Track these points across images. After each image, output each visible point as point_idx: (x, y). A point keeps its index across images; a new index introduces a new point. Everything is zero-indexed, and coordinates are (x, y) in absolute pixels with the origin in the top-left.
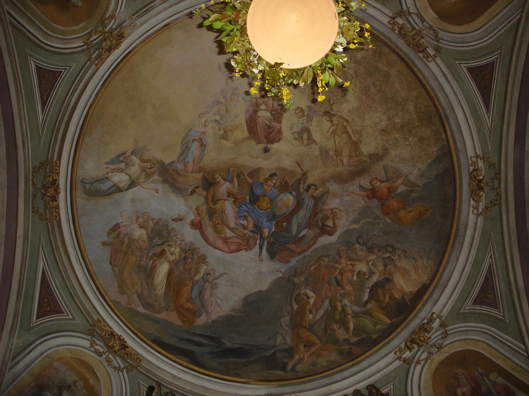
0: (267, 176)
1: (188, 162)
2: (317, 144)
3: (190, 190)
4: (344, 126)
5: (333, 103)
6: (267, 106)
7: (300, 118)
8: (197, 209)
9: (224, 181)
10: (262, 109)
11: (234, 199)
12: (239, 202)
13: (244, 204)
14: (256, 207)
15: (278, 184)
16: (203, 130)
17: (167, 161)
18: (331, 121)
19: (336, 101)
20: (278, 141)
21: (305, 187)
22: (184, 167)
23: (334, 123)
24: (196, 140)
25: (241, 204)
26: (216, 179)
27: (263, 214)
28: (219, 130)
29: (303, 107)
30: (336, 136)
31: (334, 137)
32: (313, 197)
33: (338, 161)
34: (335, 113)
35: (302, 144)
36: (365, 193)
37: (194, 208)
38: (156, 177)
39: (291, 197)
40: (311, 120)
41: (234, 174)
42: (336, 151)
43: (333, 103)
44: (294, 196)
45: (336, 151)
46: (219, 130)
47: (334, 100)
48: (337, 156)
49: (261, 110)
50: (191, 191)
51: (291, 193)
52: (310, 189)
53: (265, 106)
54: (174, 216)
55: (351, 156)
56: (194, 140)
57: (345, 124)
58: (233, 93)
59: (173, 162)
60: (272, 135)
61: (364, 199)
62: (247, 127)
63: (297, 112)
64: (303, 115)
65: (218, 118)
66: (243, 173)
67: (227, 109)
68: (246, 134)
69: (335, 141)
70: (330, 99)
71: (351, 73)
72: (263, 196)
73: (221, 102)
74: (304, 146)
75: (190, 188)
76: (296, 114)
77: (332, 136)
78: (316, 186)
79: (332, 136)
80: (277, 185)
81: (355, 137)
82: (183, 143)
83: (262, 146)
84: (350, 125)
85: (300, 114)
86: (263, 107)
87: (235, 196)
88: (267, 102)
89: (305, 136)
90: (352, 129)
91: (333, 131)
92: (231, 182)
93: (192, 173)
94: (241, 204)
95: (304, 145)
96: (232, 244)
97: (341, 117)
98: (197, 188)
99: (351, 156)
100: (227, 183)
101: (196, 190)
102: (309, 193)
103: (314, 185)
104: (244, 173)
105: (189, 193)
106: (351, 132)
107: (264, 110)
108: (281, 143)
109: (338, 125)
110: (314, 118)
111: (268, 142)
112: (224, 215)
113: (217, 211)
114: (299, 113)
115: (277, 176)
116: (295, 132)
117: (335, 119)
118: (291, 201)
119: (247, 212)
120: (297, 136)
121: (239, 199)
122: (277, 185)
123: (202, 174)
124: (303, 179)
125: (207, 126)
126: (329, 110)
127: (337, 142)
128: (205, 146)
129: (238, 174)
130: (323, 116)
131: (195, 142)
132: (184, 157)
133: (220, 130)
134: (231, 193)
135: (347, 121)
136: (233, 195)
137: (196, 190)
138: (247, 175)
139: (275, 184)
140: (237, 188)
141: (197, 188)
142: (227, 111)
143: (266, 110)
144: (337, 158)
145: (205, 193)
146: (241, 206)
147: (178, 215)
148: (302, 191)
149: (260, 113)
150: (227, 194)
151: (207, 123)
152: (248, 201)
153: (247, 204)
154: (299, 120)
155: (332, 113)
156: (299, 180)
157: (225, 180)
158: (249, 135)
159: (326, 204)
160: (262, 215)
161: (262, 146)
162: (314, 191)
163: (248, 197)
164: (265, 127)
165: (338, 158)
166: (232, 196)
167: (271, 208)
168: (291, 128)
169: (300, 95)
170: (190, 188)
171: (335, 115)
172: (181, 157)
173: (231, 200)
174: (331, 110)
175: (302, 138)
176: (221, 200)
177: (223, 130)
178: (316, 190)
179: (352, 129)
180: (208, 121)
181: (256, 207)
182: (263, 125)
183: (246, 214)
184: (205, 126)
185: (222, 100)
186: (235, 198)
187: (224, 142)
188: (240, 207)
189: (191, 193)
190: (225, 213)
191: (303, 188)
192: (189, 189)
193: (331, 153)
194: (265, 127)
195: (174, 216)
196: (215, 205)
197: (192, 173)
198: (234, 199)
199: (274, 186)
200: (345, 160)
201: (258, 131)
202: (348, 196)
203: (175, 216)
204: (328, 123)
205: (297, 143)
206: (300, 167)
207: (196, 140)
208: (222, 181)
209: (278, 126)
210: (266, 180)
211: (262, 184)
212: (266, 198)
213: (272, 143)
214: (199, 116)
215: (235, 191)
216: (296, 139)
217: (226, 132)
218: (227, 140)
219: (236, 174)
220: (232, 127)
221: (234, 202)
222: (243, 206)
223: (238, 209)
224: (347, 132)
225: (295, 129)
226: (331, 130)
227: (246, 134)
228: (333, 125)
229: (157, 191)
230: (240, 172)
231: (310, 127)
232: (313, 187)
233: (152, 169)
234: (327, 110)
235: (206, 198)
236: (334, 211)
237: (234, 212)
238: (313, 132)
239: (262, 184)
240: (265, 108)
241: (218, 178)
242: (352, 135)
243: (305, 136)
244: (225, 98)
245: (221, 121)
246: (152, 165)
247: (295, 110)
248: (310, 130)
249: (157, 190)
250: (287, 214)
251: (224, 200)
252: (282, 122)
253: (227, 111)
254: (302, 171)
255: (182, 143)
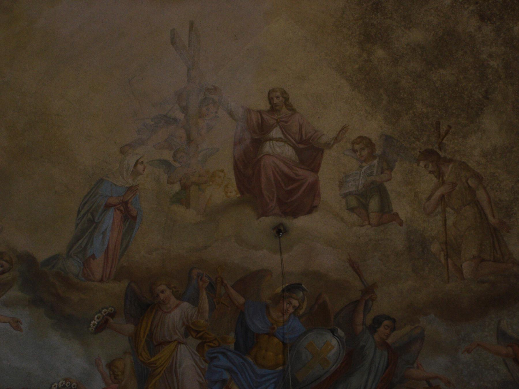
0: (279, 290)
1: (93, 257)
2: (401, 224)
3: (95, 322)
4: (469, 187)
5: (447, 132)
6: (285, 130)
7: (365, 161)
8: (110, 365)
9: (178, 298)
10: (275, 136)
11: (199, 341)
12: (211, 347)
13: (224, 354)
14: (250, 359)
15: (304, 308)
16: (131, 182)
17: (42, 256)
18: (440, 175)
19: (453, 129)
20: (310, 212)
21: (369, 322)
22: (82, 267)
23: (445, 179)
24: (115, 206)
25: (214, 353)
26: (158, 295)
27: (266, 378)
28: (169, 182)
29: (374, 137)
30: (448, 209)
31: (444, 211)
32: (385, 345)
33: (450, 267)
34: (449, 157)
35: (367, 222)
36: (510, 349)
37: (103, 363)
38: (15, 293)
39: (334, 342)
40: (391, 169)
41: (201, 283)
42: (446, 243)
43: (447, 132)
44: (339, 338)
45: (446, 243)
46: (169, 182)
47: (450, 127)
48: (447, 256)
49: (271, 139)
50: (98, 323)
51: (333, 332)
52: (379, 327)
53: (280, 132)
54: (56, 384)
55: (483, 260)
56: (108, 206)
57: (472, 182)
58: (205, 98)
59: (56, 258)
60: (293, 199)
61: (506, 364)
62: (236, 175)
63: (357, 147)
64: (372, 156)
65: (167, 155)
66: (222, 282)
67: (189, 137)
68: (234, 193)
69: (445, 221)
70: (438, 123)
71: (496, 66)
72: (267, 334)
73: (175, 120)
74: (369, 226)
75: (96, 316)
76: (355, 151)
77: (439, 209)
78: (394, 321)
79: (439, 209)
80: (301, 312)
81: (494, 216)
82: (82, 214)
83: (269, 221)
84: (485, 188)
85: (365, 153)
86: (276, 133)
87: (201, 334)
88: (286, 122)
89: (374, 204)
90: (489, 197)
91: (442, 197)
92: (195, 301)
93: (101, 281)
94: (214, 353)
95: (370, 224)
96: (136, 192)
97: (464, 166)
98: (112, 315)
99: (483, 260)
100: (186, 305)
101: (111, 320)
102: (376, 336)
103: (389, 318)
104: (225, 282)
105: (92, 327)
106: (485, 204)
107: (278, 140)
108: (316, 216)
109: (454, 185)
110: (397, 164)
111: (285, 214)
112: (175, 380)
113: (159, 370)
114: (362, 149)
115: (303, 290)
116: (350, 194)
117: (448, 170)
118: (333, 351)
119: (229, 370)
120: (354, 203)
121: (210, 342)
122: (301, 312)
123: (125, 284)
124: (364, 302)
125: (141, 174)
126: (436, 147)
127: (450, 222)
128: (135, 218)
129: (210, 283)
130: (418, 161)
131: (112, 209)
132: (83, 246)
133: (173, 183)
134: (192, 326)
135: (478, 177)
136: (198, 332)
137: (111, 320)
138: (233, 287)
139: (297, 309)
140: (207, 315)
141: (112, 315)
142: (190, 140)
143: (282, 141)
144: (447, 260)
145: (130, 328)
146: (215, 357)
147: (66, 380)
148: (360, 328)
149: (267, 147)
150: (183, 329)
151: (140, 167)
152: (232, 347)
153: (229, 353)
154: (361, 167)
155: (442, 154)
156: (356, 303)
157: (180, 297)
158: (239, 195)
159: (415, 365)
160: (264, 379)
161: (269, 221)
162: (388, 331)
163: (232, 337)
164: (280, 179)
165: (449, 260)
166: (194, 335)
167: (284, 364)
168: (341, 184)
169: (366, 110)
170: (96, 316)
171: (450, 161)
172: (78, 244)
173: (193, 342)
174: (440, 149)
175: (365, 207)
176: (170, 342)
177: (179, 183)
178: (393, 329)
179: (489, 197)
180: (142, 162)
181: (250, 359)
182: (273, 173)
183: (226, 376)
184: (135, 173)
185: (181, 116)
186: (201, 338)
187: (179, 210)
188: (212, 359)
189: (96, 328)
190: (176, 373)
191: (364, 323)
192: (93, 319)
193: (435, 248)
194: (280, 179)
195: (56, 384)
196: (154, 356)
197: (101, 281)
198: (199, 341)
199: (294, 313)
200: (467, 267)
201: (263, 186)
202: (469, 351)
203: (58, 383)
204: (432, 176)
205: (353, 218)
206: (357, 273)
207: (115, 206)
208: (173, 301)
209: (310, 178)
210: (278, 299)
211: (267, 307)
212: (276, 340)
213: (295, 214)
214: (123, 151)
215: (202, 321)
216: (352, 210)
217: (185, 187)
218: (188, 205)
219: (206, 285)
220: (200, 176)
221: (200, 348)
222: (221, 356)
223: (207, 365)
224: (476, 203)
225: (351, 187)
226: (438, 194)
227: (234, 193)
228: (443, 183)
229: (16, 324)
230: (216, 279)
231: (386, 184)
232: (386, 322)
233: (7, 275)
234: (430, 147)
235: (134, 338)
236: (432, 382)
237: (199, 370)
238: (392, 196)
239: (267, 307)
240: (281, 136)
241: (162, 292)
242: (488, 211)
243: (374, 204)
244: (185, 109)
245: (172, 162)
246: (6, 265)
247: (353, 143)
248: (385, 190)
249: (18, 321)
250: (324, 378)
251: (176, 343)
252: (321, 169)
253: (190, 140)
254: (363, 282)
255: (79, 212)
